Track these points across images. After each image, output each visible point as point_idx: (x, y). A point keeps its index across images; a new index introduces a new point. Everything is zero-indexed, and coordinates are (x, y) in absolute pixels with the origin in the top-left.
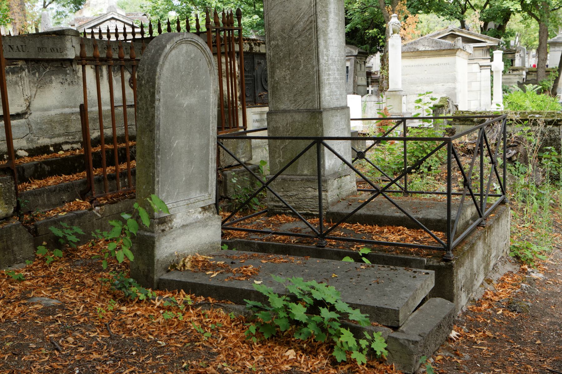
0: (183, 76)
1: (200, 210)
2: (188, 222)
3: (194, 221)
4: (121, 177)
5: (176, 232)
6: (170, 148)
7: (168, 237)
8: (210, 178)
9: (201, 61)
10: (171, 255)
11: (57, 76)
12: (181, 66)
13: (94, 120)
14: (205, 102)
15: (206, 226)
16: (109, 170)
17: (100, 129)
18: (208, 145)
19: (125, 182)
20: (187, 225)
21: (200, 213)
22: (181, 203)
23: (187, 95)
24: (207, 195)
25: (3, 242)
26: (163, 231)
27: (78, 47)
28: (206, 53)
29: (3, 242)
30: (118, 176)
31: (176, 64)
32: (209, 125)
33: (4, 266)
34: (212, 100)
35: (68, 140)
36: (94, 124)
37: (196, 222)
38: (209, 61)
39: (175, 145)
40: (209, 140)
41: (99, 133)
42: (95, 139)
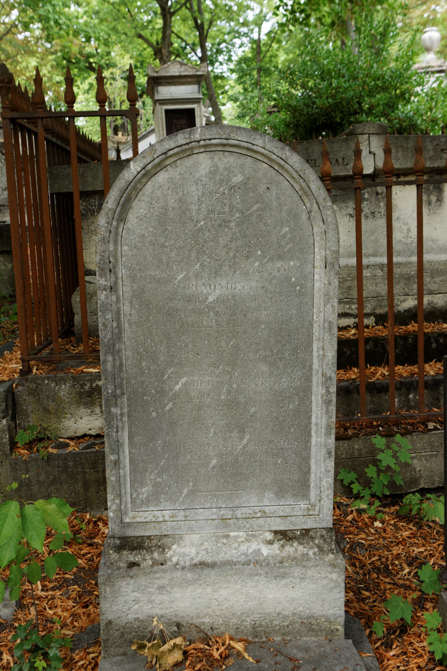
0: (200, 230)
1: (269, 536)
2: (221, 557)
3: (243, 559)
4: (398, 389)
5: (168, 576)
6: (162, 393)
7: (143, 581)
8: (313, 467)
9: (274, 191)
10: (137, 619)
11: (343, 205)
12: (194, 208)
13: (407, 278)
14: (297, 290)
15: (284, 576)
16: (403, 371)
17: (418, 295)
18: (306, 392)
19: (408, 400)
20: (213, 565)
21: (270, 543)
22: (203, 514)
23: (216, 273)
24: (303, 505)
25: (98, 472)
26: (132, 565)
27: (380, 154)
28: (287, 171)
29: (98, 472)
30: (421, 385)
31: (171, 203)
32: (310, 344)
33: (98, 507)
34: (317, 285)
35: (348, 311)
36: (406, 285)
37: (247, 563)
38: (302, 189)
39: (177, 387)
40: (309, 379)
41: (416, 302)
42: (405, 311)
